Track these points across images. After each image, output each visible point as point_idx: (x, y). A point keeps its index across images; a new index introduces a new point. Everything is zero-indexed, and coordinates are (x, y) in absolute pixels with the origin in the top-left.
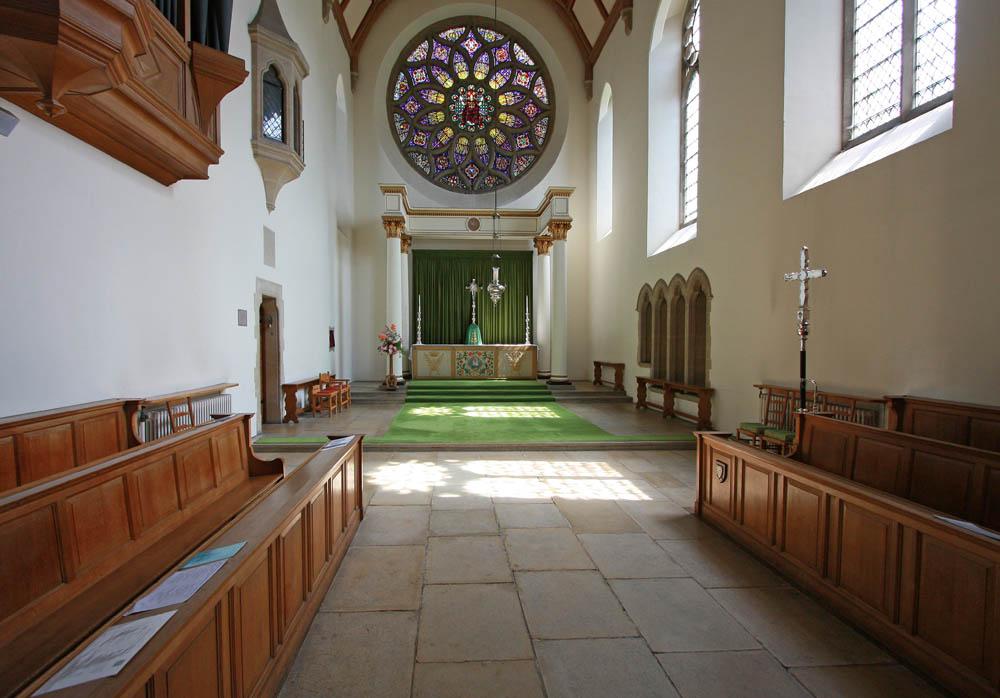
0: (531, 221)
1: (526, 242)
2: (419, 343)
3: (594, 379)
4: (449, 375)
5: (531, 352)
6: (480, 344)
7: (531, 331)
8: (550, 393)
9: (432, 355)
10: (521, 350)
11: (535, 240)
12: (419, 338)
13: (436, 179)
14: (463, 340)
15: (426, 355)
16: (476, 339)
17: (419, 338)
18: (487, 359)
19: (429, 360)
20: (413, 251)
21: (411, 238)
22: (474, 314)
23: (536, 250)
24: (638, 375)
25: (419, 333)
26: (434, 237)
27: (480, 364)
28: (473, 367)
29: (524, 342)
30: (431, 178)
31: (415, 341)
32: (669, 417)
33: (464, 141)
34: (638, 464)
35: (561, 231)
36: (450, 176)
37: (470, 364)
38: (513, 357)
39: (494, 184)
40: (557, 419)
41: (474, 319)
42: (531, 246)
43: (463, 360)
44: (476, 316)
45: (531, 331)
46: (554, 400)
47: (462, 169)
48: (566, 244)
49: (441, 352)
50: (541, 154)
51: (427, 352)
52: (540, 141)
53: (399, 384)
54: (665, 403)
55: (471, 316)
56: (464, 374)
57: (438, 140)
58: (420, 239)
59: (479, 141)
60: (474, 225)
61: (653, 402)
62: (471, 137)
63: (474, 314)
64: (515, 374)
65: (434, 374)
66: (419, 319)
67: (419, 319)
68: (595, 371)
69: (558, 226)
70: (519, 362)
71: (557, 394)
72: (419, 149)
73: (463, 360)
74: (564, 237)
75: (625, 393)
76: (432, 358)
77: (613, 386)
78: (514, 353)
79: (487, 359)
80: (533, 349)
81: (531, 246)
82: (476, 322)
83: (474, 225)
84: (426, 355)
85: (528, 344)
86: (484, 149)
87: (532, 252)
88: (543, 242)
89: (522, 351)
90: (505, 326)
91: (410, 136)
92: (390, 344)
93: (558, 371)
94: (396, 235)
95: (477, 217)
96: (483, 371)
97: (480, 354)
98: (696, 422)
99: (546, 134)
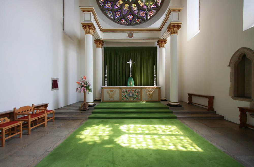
0: (156, 33)
1: (153, 43)
2: (106, 86)
3: (188, 101)
4: (118, 100)
5: (157, 90)
6: (134, 86)
7: (156, 80)
8: (172, 113)
9: (110, 91)
10: (153, 88)
11: (158, 42)
12: (106, 84)
13: (115, 20)
14: (126, 84)
15: (108, 91)
16: (132, 84)
17: (106, 84)
18: (136, 93)
19: (109, 94)
20: (104, 47)
21: (103, 41)
22: (131, 73)
23: (158, 46)
24: (188, 93)
25: (106, 81)
26: (114, 41)
27: (133, 95)
28: (130, 96)
29: (153, 85)
30: (114, 20)
31: (105, 85)
32: (190, 104)
33: (127, 5)
34: (203, 131)
35: (175, 29)
36: (121, 19)
37: (129, 95)
38: (149, 92)
39: (139, 22)
40: (198, 152)
41: (131, 76)
42: (156, 45)
43: (125, 93)
44: (132, 74)
45: (156, 80)
46: (176, 118)
47: (126, 17)
48: (178, 36)
49: (115, 90)
50: (159, 9)
51: (108, 90)
52: (159, 4)
53: (90, 106)
54: (209, 105)
55: (130, 74)
56: (126, 100)
57: (116, 5)
58: (107, 43)
59: (133, 5)
60: (131, 36)
61: (194, 102)
62: (130, 4)
63: (131, 73)
64: (150, 99)
65: (112, 100)
66: (106, 76)
67: (106, 76)
68: (241, 116)
69: (174, 26)
70: (152, 94)
71: (178, 113)
72: (108, 9)
73: (125, 93)
74: (177, 32)
75: (213, 110)
76: (110, 93)
77: (207, 108)
78: (148, 91)
79: (136, 93)
80: (159, 88)
81: (156, 45)
82: (132, 77)
83: (131, 36)
84: (108, 91)
85: (155, 86)
86: (135, 8)
87: (157, 47)
88: (162, 42)
89: (153, 89)
90: (145, 78)
91: (105, 4)
92: (84, 87)
93: (174, 99)
94: (99, 47)
95: (132, 32)
96: (135, 98)
97: (133, 91)
98: (207, 108)
99: (161, 2)
